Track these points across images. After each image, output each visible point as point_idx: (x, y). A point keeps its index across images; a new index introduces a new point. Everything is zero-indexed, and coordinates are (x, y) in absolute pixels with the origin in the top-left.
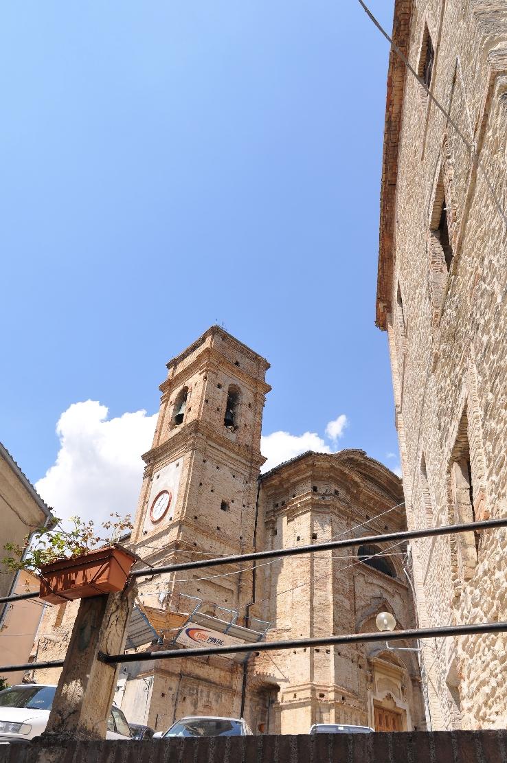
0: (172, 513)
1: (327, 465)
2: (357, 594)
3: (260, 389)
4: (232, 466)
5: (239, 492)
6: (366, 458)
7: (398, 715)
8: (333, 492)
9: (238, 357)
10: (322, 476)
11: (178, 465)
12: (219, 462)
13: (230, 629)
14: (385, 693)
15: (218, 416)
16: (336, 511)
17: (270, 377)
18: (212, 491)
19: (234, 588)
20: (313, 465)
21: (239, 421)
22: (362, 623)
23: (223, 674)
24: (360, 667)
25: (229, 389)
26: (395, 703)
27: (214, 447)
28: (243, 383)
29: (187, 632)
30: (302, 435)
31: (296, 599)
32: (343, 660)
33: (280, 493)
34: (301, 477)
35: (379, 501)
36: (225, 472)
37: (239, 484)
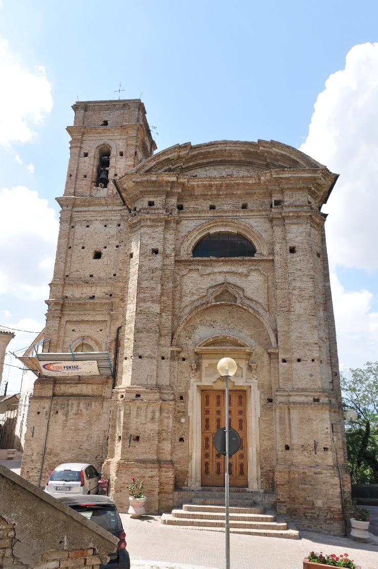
4: (102, 218)
9: (105, 116)
13: (76, 357)
16: (149, 223)
18: (83, 248)
19: (107, 318)
23: (95, 387)
27: (81, 211)
30: (314, 109)
35: (221, 186)
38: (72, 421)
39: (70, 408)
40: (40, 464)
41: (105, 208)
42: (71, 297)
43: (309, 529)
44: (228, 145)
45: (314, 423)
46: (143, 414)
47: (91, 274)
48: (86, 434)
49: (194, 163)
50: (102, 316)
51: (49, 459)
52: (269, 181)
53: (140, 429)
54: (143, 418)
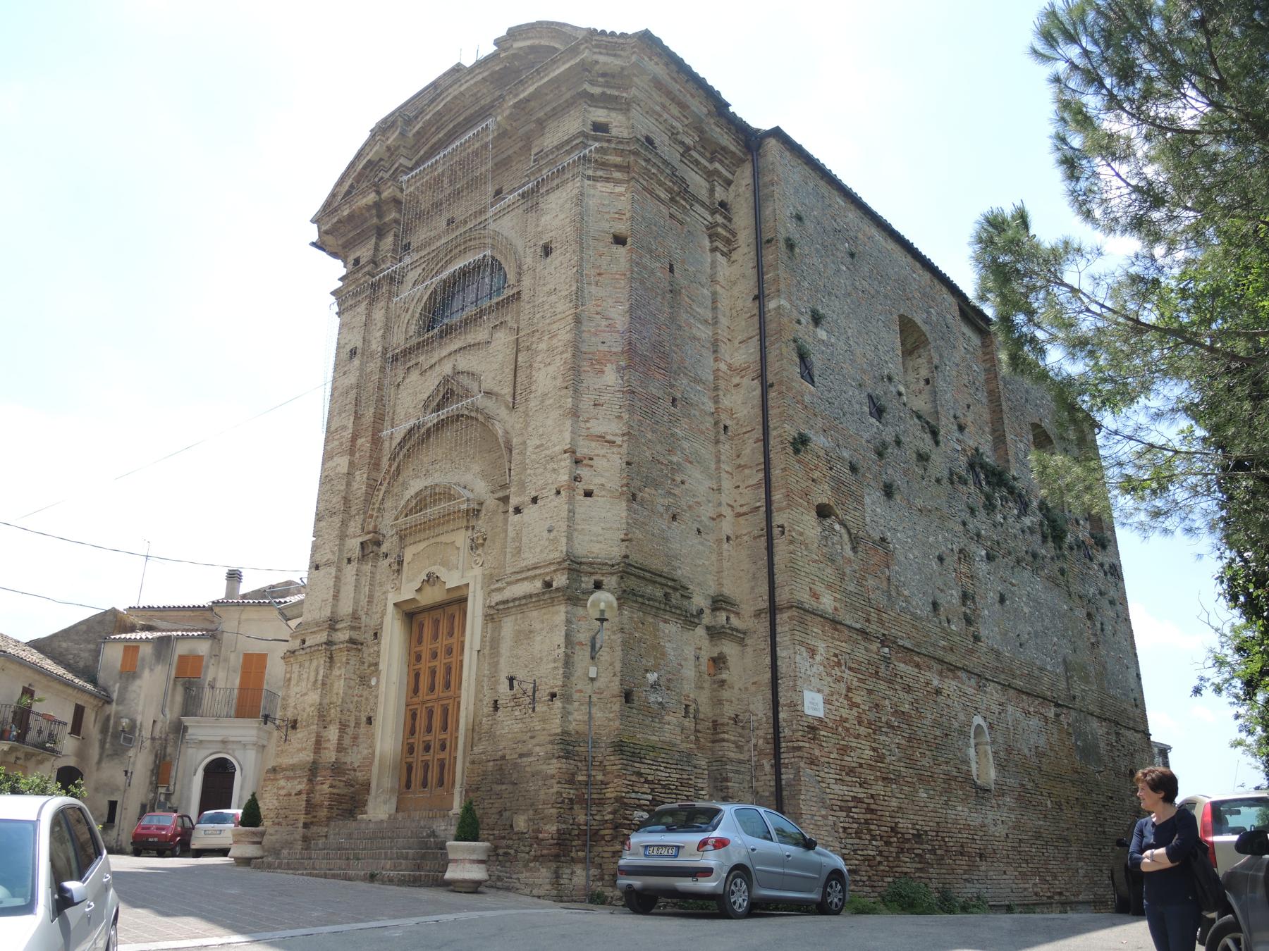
43: (499, 884)
44: (463, 81)
45: (538, 638)
49: (426, 148)
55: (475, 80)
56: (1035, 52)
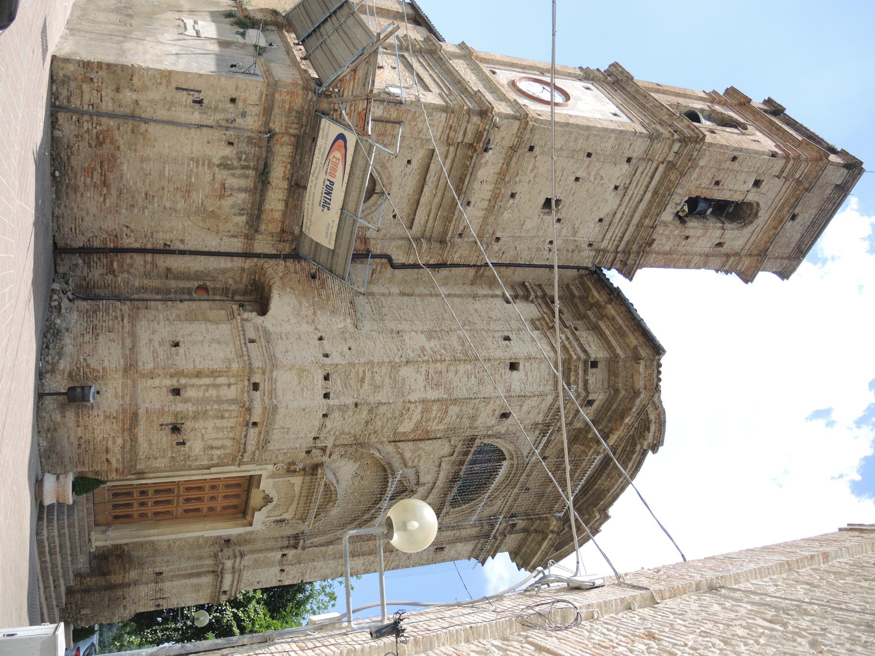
0: (533, 107)
1: (640, 383)
2: (422, 445)
3: (746, 262)
4: (618, 215)
5: (575, 233)
6: (644, 454)
7: (244, 513)
8: (590, 398)
10: (616, 375)
11: (615, 115)
12: (626, 189)
14: (273, 494)
15: (706, 182)
17: (765, 278)
18: (577, 179)
20: (637, 358)
21: (694, 226)
22: (377, 454)
23: (278, 215)
24: (308, 452)
25: (750, 204)
26: (260, 510)
27: (652, 178)
28: (758, 229)
29: (341, 137)
31: (406, 338)
32: (317, 424)
33: (576, 306)
34: (611, 338)
36: (609, 203)
37: (589, 231)
38: (208, 177)
39: (239, 172)
40: (110, 108)
41: (635, 221)
42: (483, 161)
46: (221, 435)
47: (517, 196)
48: (179, 206)
50: (422, 222)
51: (121, 129)
52: (549, 525)
53: (193, 433)
54: (213, 435)
55: (618, 484)
56: (473, 439)
